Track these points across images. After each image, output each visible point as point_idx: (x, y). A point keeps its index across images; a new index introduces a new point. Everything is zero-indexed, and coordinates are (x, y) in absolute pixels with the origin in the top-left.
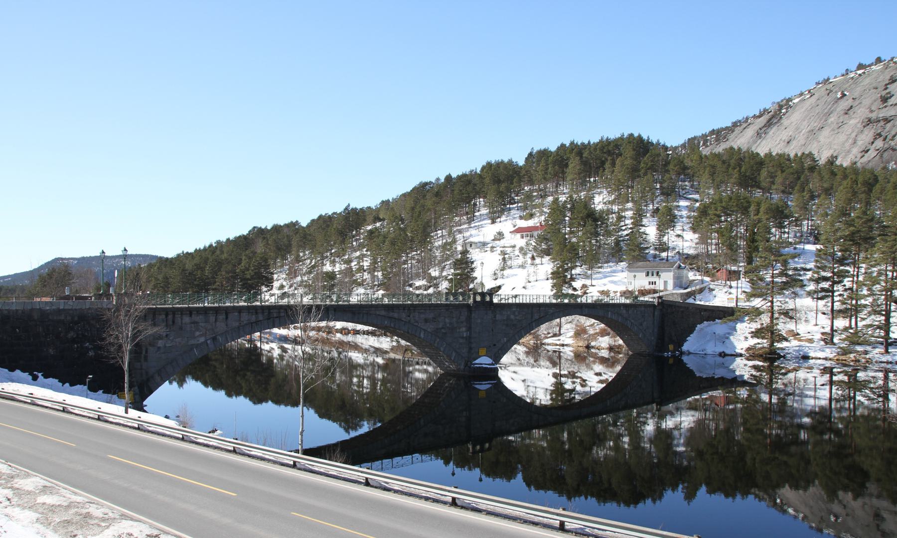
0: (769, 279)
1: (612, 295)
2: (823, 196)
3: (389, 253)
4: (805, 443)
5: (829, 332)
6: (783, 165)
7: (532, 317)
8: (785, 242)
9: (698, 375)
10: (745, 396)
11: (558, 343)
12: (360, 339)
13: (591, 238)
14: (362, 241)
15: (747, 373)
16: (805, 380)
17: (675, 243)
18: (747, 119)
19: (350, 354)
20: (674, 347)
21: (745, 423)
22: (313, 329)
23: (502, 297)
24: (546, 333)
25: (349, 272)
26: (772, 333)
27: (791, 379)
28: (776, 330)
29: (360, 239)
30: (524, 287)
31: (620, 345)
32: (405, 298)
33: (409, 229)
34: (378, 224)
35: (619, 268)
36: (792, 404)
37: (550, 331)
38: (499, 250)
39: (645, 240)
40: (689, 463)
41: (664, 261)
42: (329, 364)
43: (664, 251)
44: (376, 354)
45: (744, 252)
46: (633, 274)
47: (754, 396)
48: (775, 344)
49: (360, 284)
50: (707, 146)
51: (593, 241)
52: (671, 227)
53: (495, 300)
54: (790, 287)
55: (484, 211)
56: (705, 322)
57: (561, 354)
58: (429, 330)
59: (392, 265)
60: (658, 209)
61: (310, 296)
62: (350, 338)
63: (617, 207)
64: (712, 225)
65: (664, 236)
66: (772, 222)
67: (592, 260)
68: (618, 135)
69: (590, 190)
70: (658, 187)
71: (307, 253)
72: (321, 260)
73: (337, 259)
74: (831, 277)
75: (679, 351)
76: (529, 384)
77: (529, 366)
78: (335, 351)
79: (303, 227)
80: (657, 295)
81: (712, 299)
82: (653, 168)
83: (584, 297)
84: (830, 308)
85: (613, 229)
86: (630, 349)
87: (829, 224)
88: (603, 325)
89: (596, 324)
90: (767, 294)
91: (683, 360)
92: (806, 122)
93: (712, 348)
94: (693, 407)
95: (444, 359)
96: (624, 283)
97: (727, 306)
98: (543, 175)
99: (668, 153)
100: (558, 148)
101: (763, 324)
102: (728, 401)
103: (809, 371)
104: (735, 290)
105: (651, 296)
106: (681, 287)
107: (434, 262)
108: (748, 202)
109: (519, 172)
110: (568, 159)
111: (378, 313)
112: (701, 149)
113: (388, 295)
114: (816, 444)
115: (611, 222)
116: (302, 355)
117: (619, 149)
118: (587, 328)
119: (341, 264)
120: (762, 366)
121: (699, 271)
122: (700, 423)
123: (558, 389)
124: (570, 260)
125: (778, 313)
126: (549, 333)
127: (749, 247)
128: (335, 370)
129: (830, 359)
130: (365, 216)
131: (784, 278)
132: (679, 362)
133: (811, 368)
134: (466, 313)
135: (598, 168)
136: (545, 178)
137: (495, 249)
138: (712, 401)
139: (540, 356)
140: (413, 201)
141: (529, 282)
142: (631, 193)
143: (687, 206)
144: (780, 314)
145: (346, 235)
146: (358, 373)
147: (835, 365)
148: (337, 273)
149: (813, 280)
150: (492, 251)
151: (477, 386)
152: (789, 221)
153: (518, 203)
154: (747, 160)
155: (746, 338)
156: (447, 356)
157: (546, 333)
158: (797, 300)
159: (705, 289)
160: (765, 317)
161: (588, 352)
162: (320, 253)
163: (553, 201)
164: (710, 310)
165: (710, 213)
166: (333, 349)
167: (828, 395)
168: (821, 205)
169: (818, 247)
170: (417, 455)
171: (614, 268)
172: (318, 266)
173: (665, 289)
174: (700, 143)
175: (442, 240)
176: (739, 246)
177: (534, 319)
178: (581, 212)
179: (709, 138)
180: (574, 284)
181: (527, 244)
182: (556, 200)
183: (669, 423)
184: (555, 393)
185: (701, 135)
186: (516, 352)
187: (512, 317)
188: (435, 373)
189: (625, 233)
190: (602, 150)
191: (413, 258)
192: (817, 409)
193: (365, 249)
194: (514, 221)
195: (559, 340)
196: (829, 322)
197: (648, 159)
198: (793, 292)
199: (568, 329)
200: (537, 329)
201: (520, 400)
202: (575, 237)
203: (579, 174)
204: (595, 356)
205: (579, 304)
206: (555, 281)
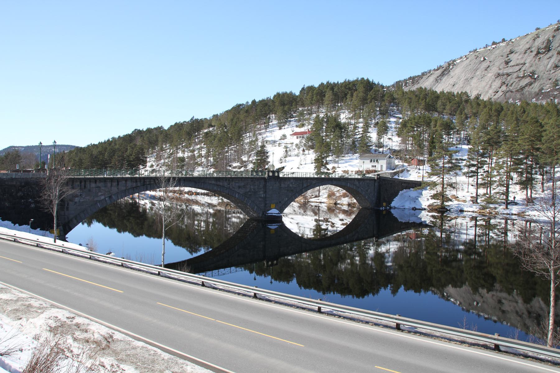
0: (441, 165)
2: (472, 117)
3: (217, 146)
4: (460, 261)
6: (450, 99)
7: (303, 186)
10: (427, 233)
12: (199, 198)
13: (338, 139)
14: (201, 139)
17: (387, 143)
18: (430, 71)
19: (193, 207)
21: (427, 248)
22: (171, 191)
24: (311, 195)
25: (193, 157)
26: (443, 196)
28: (445, 195)
29: (200, 138)
30: (298, 168)
31: (354, 203)
34: (211, 129)
37: (313, 194)
38: (283, 145)
40: (394, 272)
41: (381, 153)
42: (180, 213)
44: (209, 207)
45: (428, 149)
46: (363, 161)
47: (432, 233)
49: (200, 165)
50: (407, 86)
51: (339, 141)
53: (281, 175)
54: (453, 170)
55: (275, 122)
56: (404, 190)
57: (320, 208)
58: (241, 193)
60: (378, 123)
61: (169, 172)
62: (193, 197)
63: (354, 121)
64: (409, 133)
66: (444, 132)
67: (338, 152)
68: (355, 79)
69: (338, 111)
71: (168, 145)
72: (176, 150)
73: (186, 150)
74: (476, 164)
76: (301, 225)
77: (301, 215)
78: (184, 205)
79: (165, 130)
80: (376, 173)
81: (408, 175)
82: (375, 99)
83: (334, 174)
84: (476, 183)
85: (351, 134)
87: (476, 133)
88: (344, 191)
89: (340, 190)
90: (440, 174)
91: (391, 212)
93: (408, 205)
94: (397, 240)
95: (250, 210)
97: (417, 180)
98: (310, 101)
99: (384, 89)
100: (320, 85)
101: (437, 191)
102: (417, 236)
103: (464, 218)
105: (373, 174)
106: (391, 169)
107: (245, 152)
108: (430, 120)
109: (296, 99)
110: (325, 92)
111: (210, 182)
112: (403, 88)
113: (217, 171)
114: (467, 261)
116: (164, 207)
117: (356, 87)
118: (335, 192)
120: (437, 216)
121: (401, 160)
123: (318, 229)
124: (326, 152)
126: (312, 195)
127: (430, 146)
128: (184, 216)
129: (476, 212)
132: (389, 213)
134: (263, 183)
135: (343, 98)
136: (311, 103)
137: (281, 145)
138: (408, 236)
139: (307, 209)
141: (301, 165)
142: (362, 113)
143: (395, 122)
144: (448, 185)
145: (192, 135)
146: (198, 218)
147: (478, 215)
148: (186, 158)
149: (467, 166)
150: (279, 146)
151: (269, 227)
154: (430, 95)
156: (252, 209)
157: (311, 195)
158: (457, 177)
161: (336, 207)
162: (175, 145)
164: (407, 183)
166: (183, 204)
167: (474, 233)
168: (471, 122)
169: (470, 147)
170: (233, 268)
171: (351, 157)
172: (174, 154)
173: (382, 170)
174: (402, 84)
176: (424, 145)
177: (303, 187)
179: (408, 81)
180: (328, 166)
181: (300, 142)
182: (318, 117)
183: (383, 249)
186: (293, 207)
187: (291, 185)
188: (245, 219)
189: (358, 136)
191: (231, 150)
192: (468, 241)
193: (203, 144)
194: (293, 128)
195: (319, 199)
196: (475, 190)
197: (372, 93)
198: (455, 173)
200: (305, 193)
201: (295, 235)
203: (332, 101)
204: (340, 209)
206: (316, 164)
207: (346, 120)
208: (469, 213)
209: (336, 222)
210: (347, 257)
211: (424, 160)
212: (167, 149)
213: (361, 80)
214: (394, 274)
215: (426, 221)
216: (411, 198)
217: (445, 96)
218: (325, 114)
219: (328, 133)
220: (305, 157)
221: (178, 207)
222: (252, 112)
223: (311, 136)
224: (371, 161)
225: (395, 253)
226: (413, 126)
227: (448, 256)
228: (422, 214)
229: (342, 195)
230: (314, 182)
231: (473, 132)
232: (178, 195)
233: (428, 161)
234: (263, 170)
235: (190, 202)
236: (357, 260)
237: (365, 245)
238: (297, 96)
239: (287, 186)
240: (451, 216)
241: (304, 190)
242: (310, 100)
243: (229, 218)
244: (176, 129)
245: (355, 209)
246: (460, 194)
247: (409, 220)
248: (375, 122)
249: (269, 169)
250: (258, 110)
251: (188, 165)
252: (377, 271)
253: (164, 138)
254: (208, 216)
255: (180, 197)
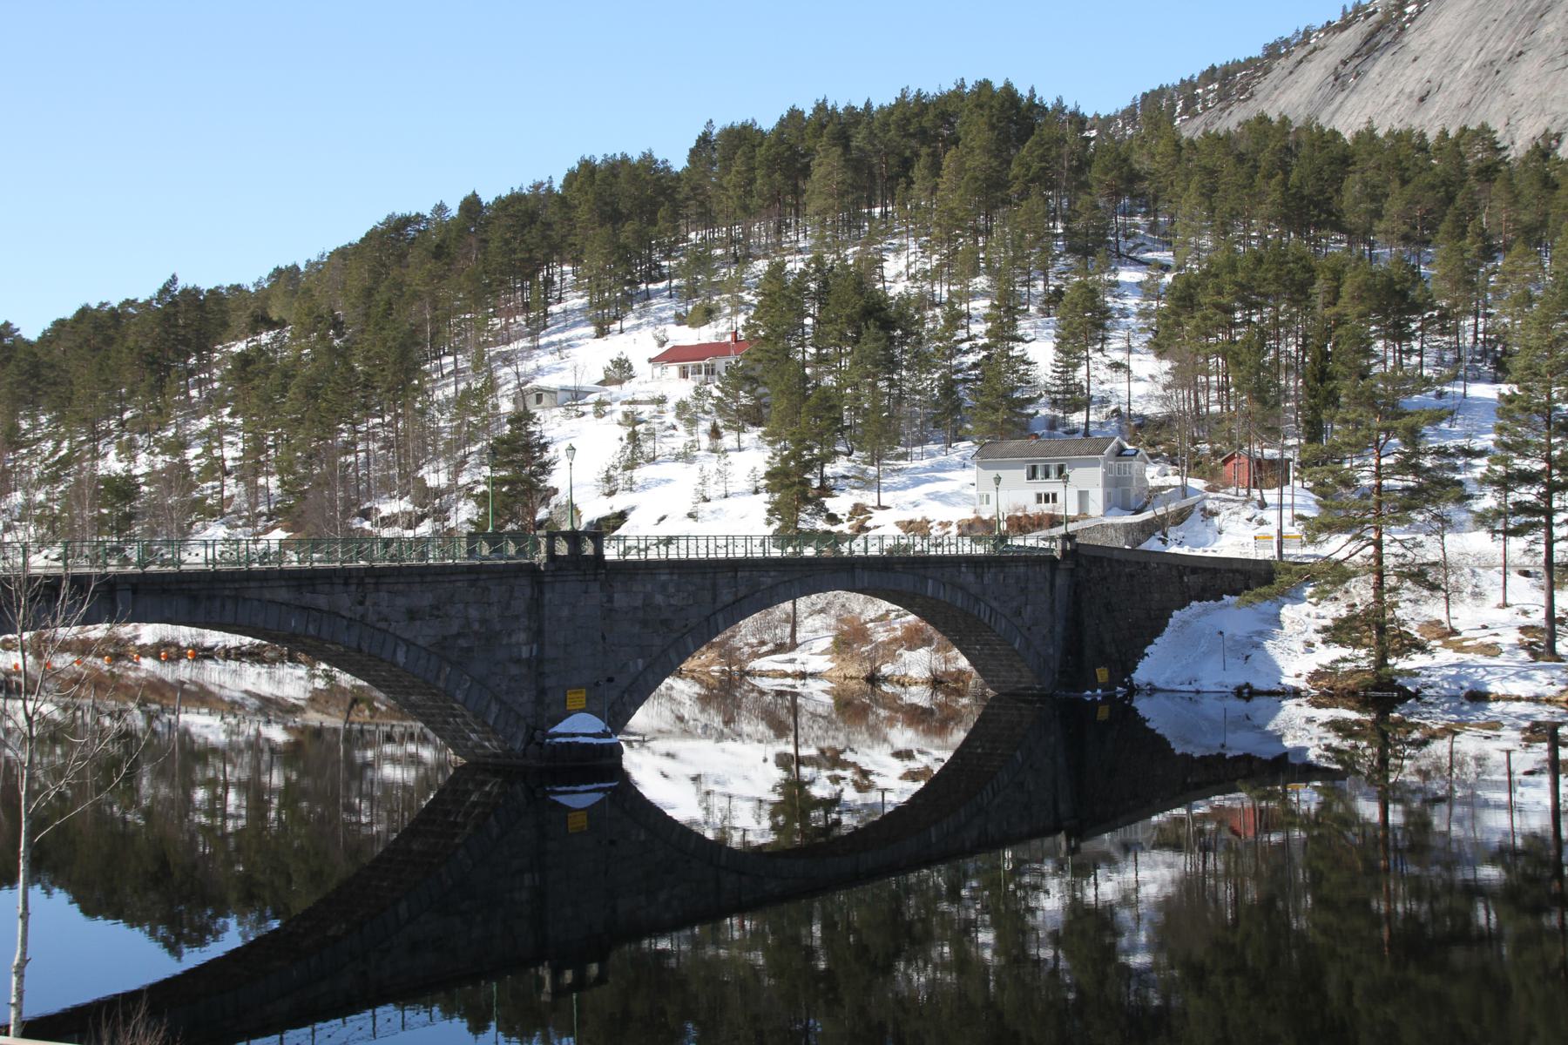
0: (1368, 484)
1: (936, 532)
2: (1518, 248)
3: (299, 422)
4: (1489, 938)
5: (1543, 624)
6: (1405, 164)
7: (714, 600)
8: (1412, 378)
9: (1178, 752)
10: (1313, 807)
11: (790, 671)
12: (215, 674)
13: (875, 375)
14: (216, 385)
15: (1316, 742)
16: (1480, 760)
17: (1107, 387)
18: (1307, 34)
19: (183, 717)
20: (1110, 673)
21: (1317, 879)
22: (65, 647)
23: (628, 543)
24: (754, 641)
25: (178, 476)
26: (1382, 630)
27: (1439, 758)
28: (1391, 621)
29: (211, 381)
30: (691, 515)
31: (961, 672)
32: (349, 551)
33: (358, 351)
34: (265, 338)
35: (955, 458)
36: (1444, 828)
37: (766, 637)
38: (618, 410)
39: (1025, 380)
40: (1166, 998)
41: (1078, 436)
42: (115, 750)
43: (1077, 408)
44: (266, 715)
45: (1299, 408)
46: (993, 473)
47: (1339, 808)
48: (1390, 662)
49: (215, 513)
50: (1195, 115)
51: (880, 384)
52: (1094, 340)
53: (611, 554)
54: (1427, 501)
55: (575, 301)
56: (1194, 603)
57: (799, 700)
58: (420, 642)
59: (311, 457)
60: (1059, 293)
61: (56, 551)
62: (184, 671)
63: (945, 288)
64: (1208, 335)
65: (1076, 366)
66: (1374, 323)
67: (878, 437)
68: (949, 86)
69: (870, 240)
70: (1060, 231)
71: (43, 419)
72: (89, 440)
73: (141, 440)
74: (1543, 471)
75: (1124, 685)
76: (711, 787)
77: (710, 737)
78: (137, 712)
79: (28, 343)
80: (1060, 530)
81: (1211, 537)
82: (1044, 179)
83: (860, 540)
84: (1541, 559)
85: (937, 349)
86: (989, 683)
87: (1535, 325)
88: (912, 618)
89: (893, 615)
90: (1363, 523)
91: (1135, 710)
92: (1474, 37)
93: (1217, 675)
94: (1170, 841)
95: (466, 724)
96: (968, 499)
97: (1252, 557)
98: (739, 197)
99: (1087, 134)
100: (782, 123)
101: (1354, 605)
102: (1267, 822)
103: (1490, 733)
104: (1275, 513)
105: (1044, 533)
106: (1126, 508)
107: (435, 445)
108: (1310, 270)
109: (674, 189)
110: (810, 153)
112: (1178, 122)
113: (300, 542)
114: (1524, 941)
115: (929, 331)
116: (26, 729)
117: (952, 124)
118: (869, 626)
119: (152, 453)
120: (1357, 722)
121: (1173, 463)
122: (1191, 889)
123: (794, 800)
124: (820, 437)
125: (1396, 574)
126: (763, 643)
127: (1312, 392)
128: (135, 766)
129: (1549, 701)
130: (226, 312)
131: (1410, 477)
132: (1125, 715)
133: (1495, 725)
134: (528, 591)
135: (893, 178)
136: (745, 208)
137: (607, 408)
138: (1220, 823)
139: (739, 707)
140: (370, 271)
141: (706, 500)
142: (984, 249)
143: (1139, 284)
144: (1401, 576)
145: (168, 368)
146: (210, 773)
147: (1562, 716)
148: (142, 480)
149: (1492, 483)
150: (599, 414)
151: (562, 799)
152: (1423, 320)
153: (670, 277)
154: (1304, 151)
155: (1309, 645)
156: (476, 717)
157: (754, 641)
158: (1449, 537)
159: (1191, 512)
160: (1360, 585)
161: (873, 693)
162: (85, 420)
163: (769, 273)
164: (1205, 570)
165: (1203, 300)
166: (132, 705)
167: (1548, 801)
168: (1513, 273)
169: (1505, 389)
170: (387, 1012)
171: (940, 458)
172: (80, 460)
173: (1083, 515)
174: (1174, 106)
175: (456, 383)
176: (1283, 393)
177: (719, 605)
178: (847, 302)
179: (1200, 91)
180: (831, 504)
181: (699, 394)
182: (777, 271)
183: (1105, 888)
184: (784, 812)
185: (1178, 83)
186: (671, 699)
187: (659, 599)
188: (441, 766)
189: (971, 359)
190: (904, 128)
191: (370, 436)
192: (1519, 842)
193: (228, 410)
194: (661, 328)
195: (792, 661)
196: (1542, 598)
197: (1031, 152)
198: (1435, 517)
199: (815, 631)
200: (728, 633)
201: (683, 834)
202: (831, 373)
203: (842, 195)
204: (892, 703)
205: (846, 559)
206: (777, 496)
207: (908, 284)
208: (1516, 704)
209: (875, 763)
210: (937, 931)
211: (1281, 459)
212: (39, 440)
213: (979, 94)
214: (1164, 1010)
215: (1306, 749)
216: (1229, 643)
217: (1381, 151)
218: (811, 260)
219: (828, 347)
220: (723, 461)
221: (107, 722)
222: (466, 257)
223: (750, 363)
224: (1032, 475)
225: (1166, 905)
226: (1224, 301)
227: (1422, 919)
228: (1281, 717)
229: (902, 638)
230: (769, 581)
231: (1520, 317)
232: (103, 664)
233: (1303, 464)
234: (523, 528)
235: (169, 694)
236: (985, 945)
237: (1017, 871)
238: (678, 177)
239: (639, 603)
240: (1428, 722)
241: (720, 617)
242: (740, 192)
243: (368, 765)
244: (87, 341)
245: (965, 701)
246: (1465, 616)
247: (1223, 746)
248: (1046, 291)
249: (554, 524)
250: (492, 246)
251: (154, 516)
252: (1081, 992)
253: (21, 384)
254: (259, 764)
255: (112, 674)
